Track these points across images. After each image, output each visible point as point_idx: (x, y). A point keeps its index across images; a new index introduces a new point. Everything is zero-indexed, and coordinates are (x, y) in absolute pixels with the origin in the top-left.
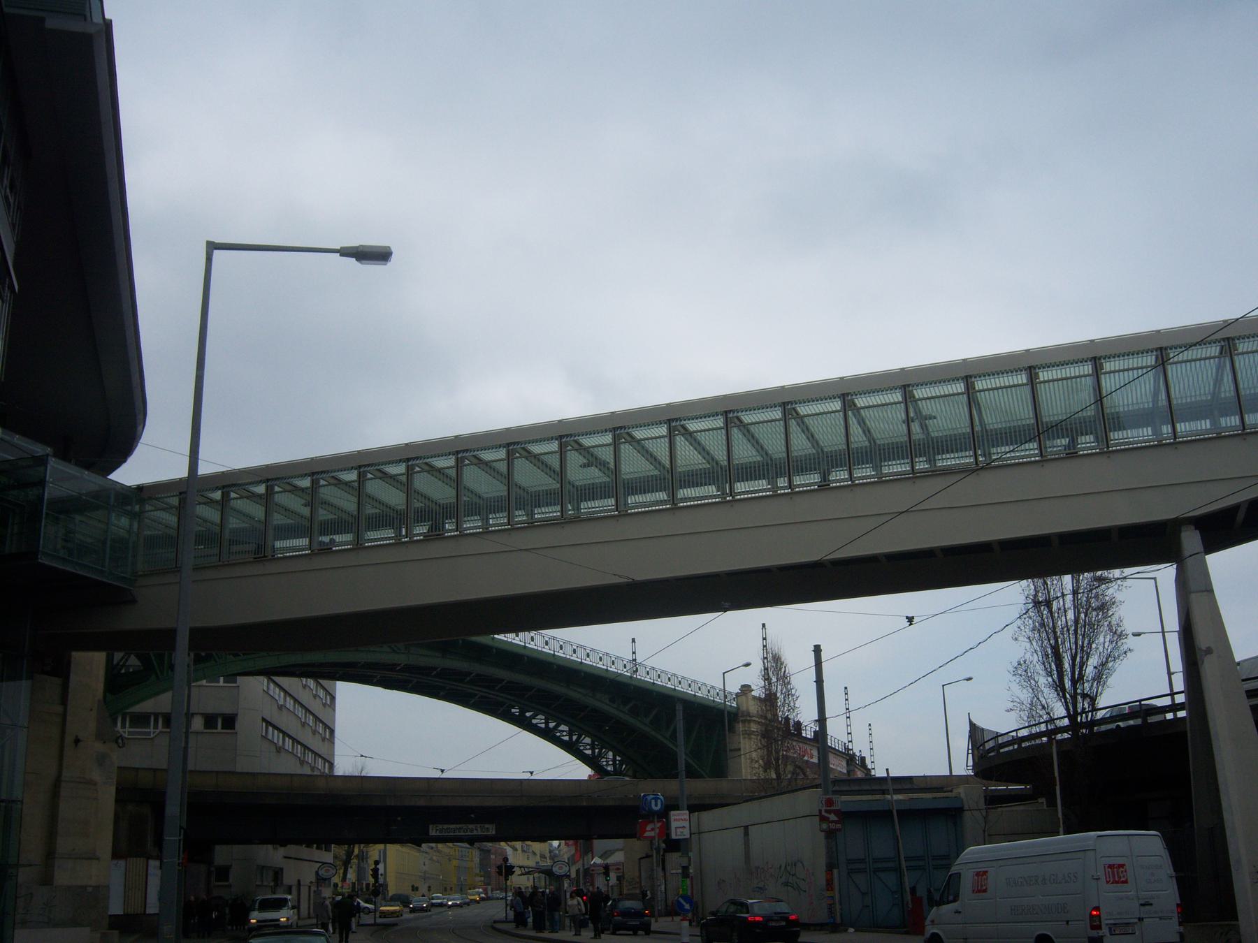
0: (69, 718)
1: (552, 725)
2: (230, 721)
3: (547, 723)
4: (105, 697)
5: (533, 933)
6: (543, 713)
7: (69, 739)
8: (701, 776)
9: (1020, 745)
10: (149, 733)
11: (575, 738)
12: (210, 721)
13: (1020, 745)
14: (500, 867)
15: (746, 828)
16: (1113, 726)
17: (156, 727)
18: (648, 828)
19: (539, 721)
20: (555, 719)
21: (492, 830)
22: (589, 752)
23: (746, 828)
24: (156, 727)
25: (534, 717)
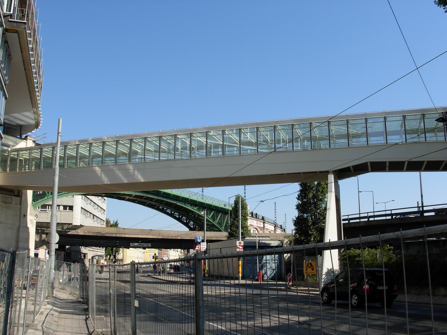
0: (22, 209)
1: (173, 212)
2: (71, 208)
3: (171, 212)
4: (32, 203)
5: (243, 282)
6: (170, 209)
7: (22, 215)
8: (220, 231)
9: (349, 221)
10: (46, 211)
11: (180, 217)
12: (65, 207)
13: (368, 219)
14: (153, 257)
15: (221, 249)
16: (358, 220)
17: (48, 209)
18: (197, 246)
19: (169, 211)
20: (174, 211)
21: (150, 245)
22: (185, 221)
23: (221, 249)
24: (48, 209)
25: (167, 210)
